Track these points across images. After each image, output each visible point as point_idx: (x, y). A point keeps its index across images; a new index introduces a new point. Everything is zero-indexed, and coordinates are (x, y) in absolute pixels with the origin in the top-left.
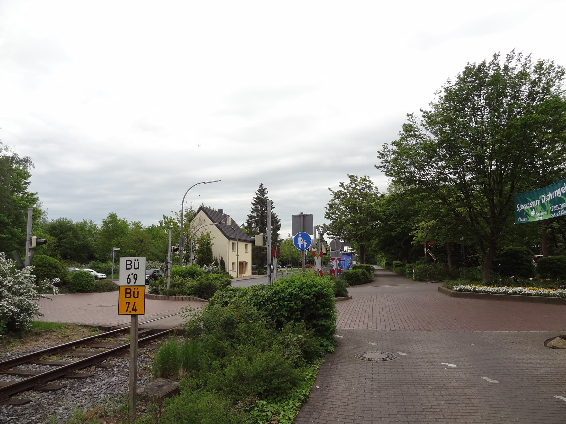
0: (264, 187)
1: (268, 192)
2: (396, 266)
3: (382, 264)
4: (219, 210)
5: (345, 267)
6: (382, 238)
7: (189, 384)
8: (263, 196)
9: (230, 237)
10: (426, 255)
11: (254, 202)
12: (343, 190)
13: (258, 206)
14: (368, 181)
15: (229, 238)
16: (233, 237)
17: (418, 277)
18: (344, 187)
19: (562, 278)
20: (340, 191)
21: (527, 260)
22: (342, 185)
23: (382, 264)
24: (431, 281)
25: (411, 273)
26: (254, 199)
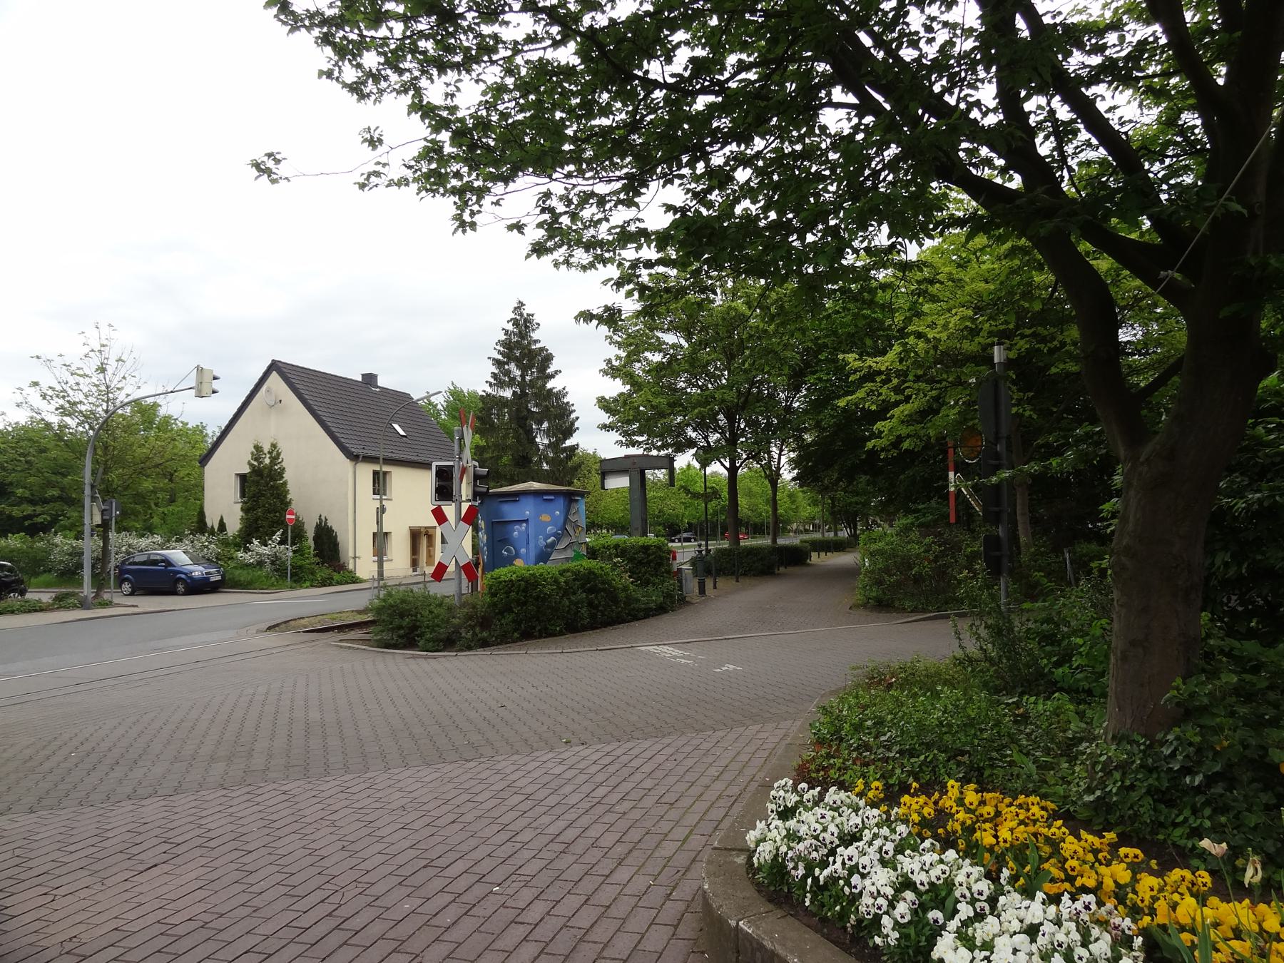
1: (538, 324)
4: (363, 375)
5: (528, 549)
9: (355, 451)
11: (500, 357)
15: (354, 458)
16: (365, 452)
19: (1282, 477)
21: (508, 593)
24: (924, 611)
26: (498, 347)
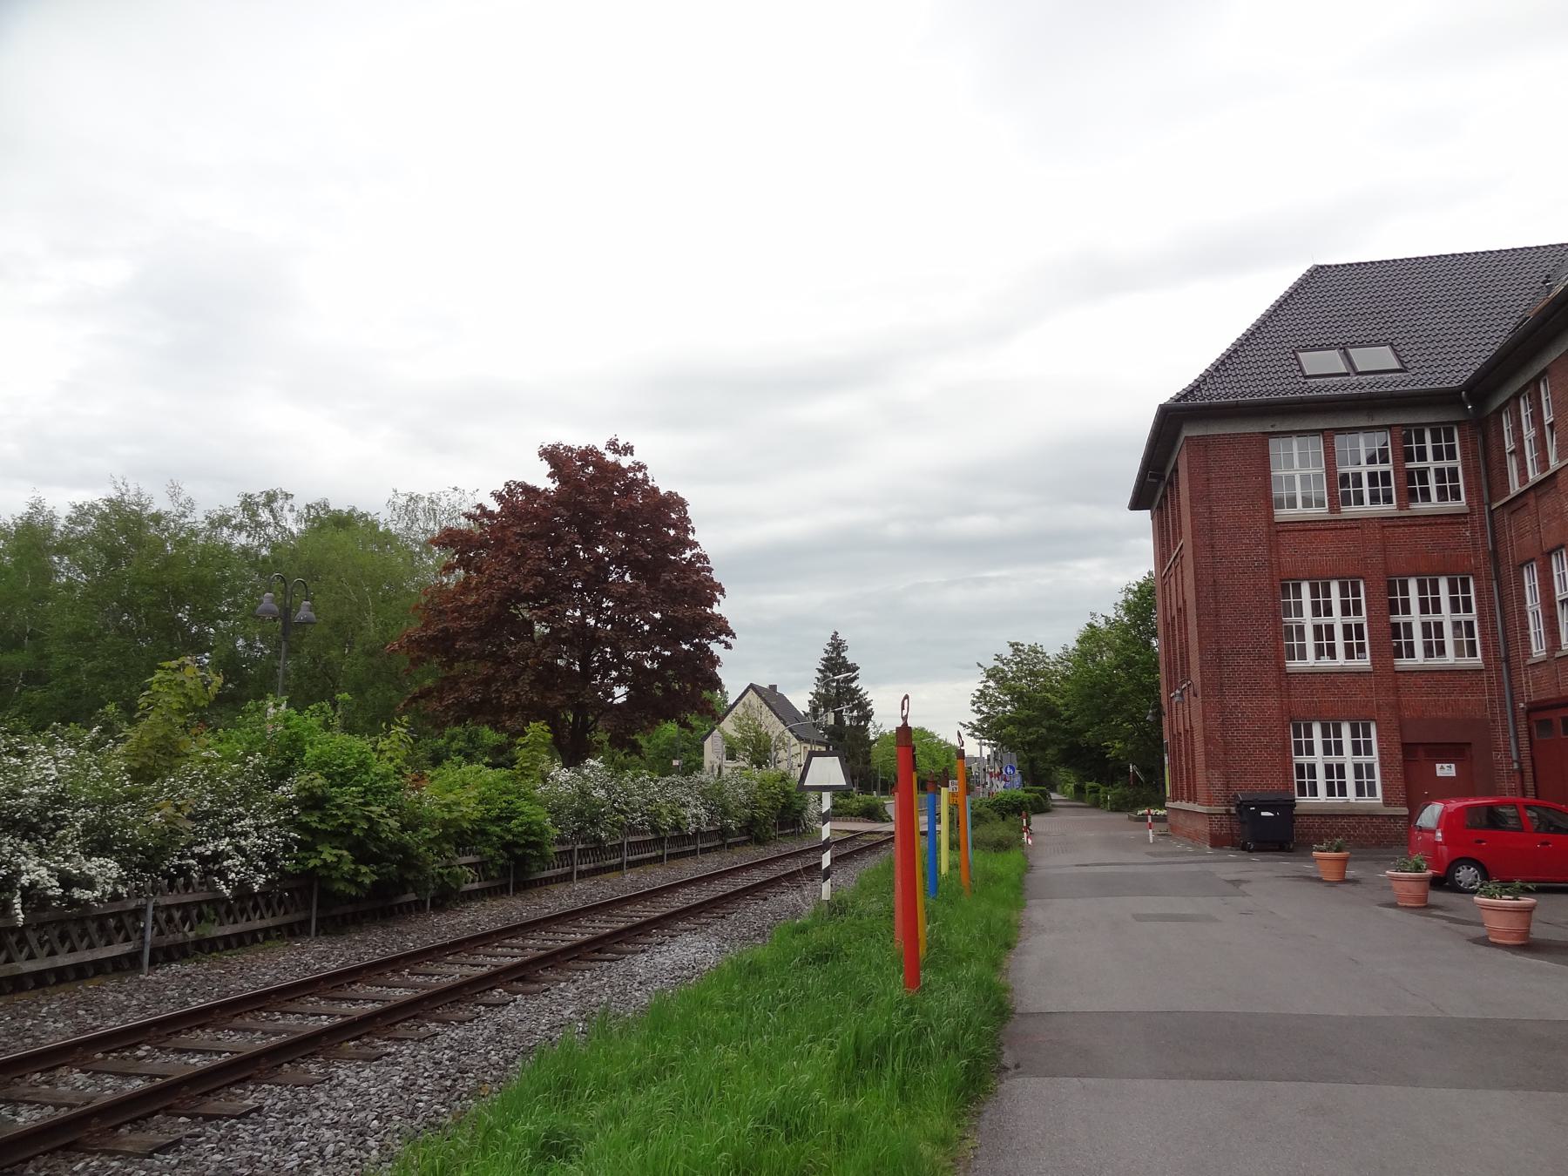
0: (840, 637)
2: (1090, 792)
3: (1068, 790)
6: (1064, 747)
7: (513, 1145)
8: (839, 654)
10: (1131, 776)
12: (1001, 666)
13: (828, 674)
14: (1042, 653)
17: (1114, 806)
18: (1002, 661)
20: (995, 667)
22: (998, 658)
23: (1068, 790)
25: (1106, 801)
